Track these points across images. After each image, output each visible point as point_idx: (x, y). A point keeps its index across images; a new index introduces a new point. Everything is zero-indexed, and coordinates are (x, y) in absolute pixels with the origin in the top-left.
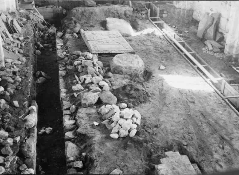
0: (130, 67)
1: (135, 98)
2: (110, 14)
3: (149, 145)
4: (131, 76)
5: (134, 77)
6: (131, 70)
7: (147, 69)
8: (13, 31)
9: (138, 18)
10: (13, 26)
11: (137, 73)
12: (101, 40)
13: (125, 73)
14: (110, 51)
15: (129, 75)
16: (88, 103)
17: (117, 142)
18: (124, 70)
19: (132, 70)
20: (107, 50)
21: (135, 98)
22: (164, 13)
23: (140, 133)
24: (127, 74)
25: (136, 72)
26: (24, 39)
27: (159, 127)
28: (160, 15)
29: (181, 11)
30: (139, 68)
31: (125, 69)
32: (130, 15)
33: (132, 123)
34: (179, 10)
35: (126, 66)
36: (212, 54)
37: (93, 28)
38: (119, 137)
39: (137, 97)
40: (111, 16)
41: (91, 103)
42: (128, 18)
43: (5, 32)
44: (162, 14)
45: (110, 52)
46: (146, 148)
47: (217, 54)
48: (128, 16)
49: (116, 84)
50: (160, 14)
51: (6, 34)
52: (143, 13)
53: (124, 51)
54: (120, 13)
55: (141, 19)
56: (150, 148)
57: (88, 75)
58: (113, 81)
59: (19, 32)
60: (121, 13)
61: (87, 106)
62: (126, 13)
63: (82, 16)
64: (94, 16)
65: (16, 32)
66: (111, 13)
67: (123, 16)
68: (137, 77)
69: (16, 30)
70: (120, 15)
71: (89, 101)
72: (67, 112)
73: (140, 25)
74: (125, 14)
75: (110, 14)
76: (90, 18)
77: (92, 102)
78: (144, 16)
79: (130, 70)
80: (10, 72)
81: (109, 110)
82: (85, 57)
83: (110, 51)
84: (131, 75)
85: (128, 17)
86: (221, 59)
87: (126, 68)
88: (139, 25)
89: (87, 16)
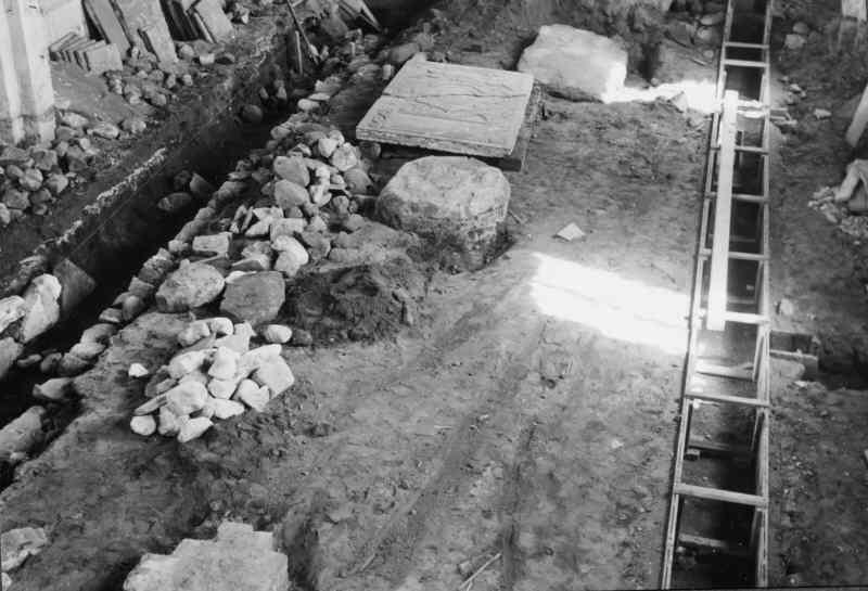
0: (431, 208)
1: (342, 316)
2: (576, 14)
3: (216, 486)
4: (430, 242)
5: (441, 247)
6: (431, 218)
7: (510, 228)
8: (196, 34)
9: (673, 40)
10: (196, 15)
11: (456, 233)
12: (434, 101)
13: (409, 225)
14: (423, 142)
15: (422, 236)
16: (173, 299)
17: (139, 445)
18: (406, 215)
19: (436, 219)
20: (409, 137)
21: (342, 316)
22: (792, 33)
23: (217, 435)
24: (414, 230)
25: (450, 228)
26: (216, 61)
27: (320, 436)
28: (771, 37)
29: (859, 28)
30: (463, 216)
31: (410, 213)
32: (647, 23)
33: (231, 398)
34: (849, 24)
35: (415, 200)
36: (831, 218)
37: (473, 57)
38: (156, 433)
39: (350, 315)
40: (577, 20)
41: (183, 302)
42: (639, 37)
43: (144, 33)
44: (784, 35)
45: (423, 146)
46: (201, 492)
47: (856, 220)
48: (638, 25)
49: (670, 255)
50: (773, 30)
51: (148, 39)
52: (707, 21)
53: (474, 148)
54: (612, 13)
55: (685, 42)
56: (212, 496)
57: (273, 209)
58: (343, 247)
59: (213, 38)
60: (615, 13)
61: (170, 309)
62: (634, 15)
63: (466, 10)
64: (511, 14)
65: (204, 38)
66: (579, 9)
67: (622, 25)
68: (456, 251)
69: (202, 24)
70: (611, 20)
71: (179, 294)
72: (111, 316)
73: (665, 66)
74: (631, 20)
75: (576, 14)
76: (493, 18)
77: (185, 299)
78: (704, 35)
79: (426, 219)
80: (39, 156)
81: (198, 337)
82: (311, 148)
83: (419, 140)
84: (430, 238)
85: (638, 31)
86: (857, 243)
87: (414, 208)
88: (660, 64)
89: (485, 12)
